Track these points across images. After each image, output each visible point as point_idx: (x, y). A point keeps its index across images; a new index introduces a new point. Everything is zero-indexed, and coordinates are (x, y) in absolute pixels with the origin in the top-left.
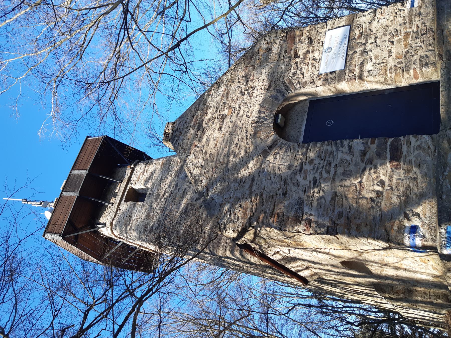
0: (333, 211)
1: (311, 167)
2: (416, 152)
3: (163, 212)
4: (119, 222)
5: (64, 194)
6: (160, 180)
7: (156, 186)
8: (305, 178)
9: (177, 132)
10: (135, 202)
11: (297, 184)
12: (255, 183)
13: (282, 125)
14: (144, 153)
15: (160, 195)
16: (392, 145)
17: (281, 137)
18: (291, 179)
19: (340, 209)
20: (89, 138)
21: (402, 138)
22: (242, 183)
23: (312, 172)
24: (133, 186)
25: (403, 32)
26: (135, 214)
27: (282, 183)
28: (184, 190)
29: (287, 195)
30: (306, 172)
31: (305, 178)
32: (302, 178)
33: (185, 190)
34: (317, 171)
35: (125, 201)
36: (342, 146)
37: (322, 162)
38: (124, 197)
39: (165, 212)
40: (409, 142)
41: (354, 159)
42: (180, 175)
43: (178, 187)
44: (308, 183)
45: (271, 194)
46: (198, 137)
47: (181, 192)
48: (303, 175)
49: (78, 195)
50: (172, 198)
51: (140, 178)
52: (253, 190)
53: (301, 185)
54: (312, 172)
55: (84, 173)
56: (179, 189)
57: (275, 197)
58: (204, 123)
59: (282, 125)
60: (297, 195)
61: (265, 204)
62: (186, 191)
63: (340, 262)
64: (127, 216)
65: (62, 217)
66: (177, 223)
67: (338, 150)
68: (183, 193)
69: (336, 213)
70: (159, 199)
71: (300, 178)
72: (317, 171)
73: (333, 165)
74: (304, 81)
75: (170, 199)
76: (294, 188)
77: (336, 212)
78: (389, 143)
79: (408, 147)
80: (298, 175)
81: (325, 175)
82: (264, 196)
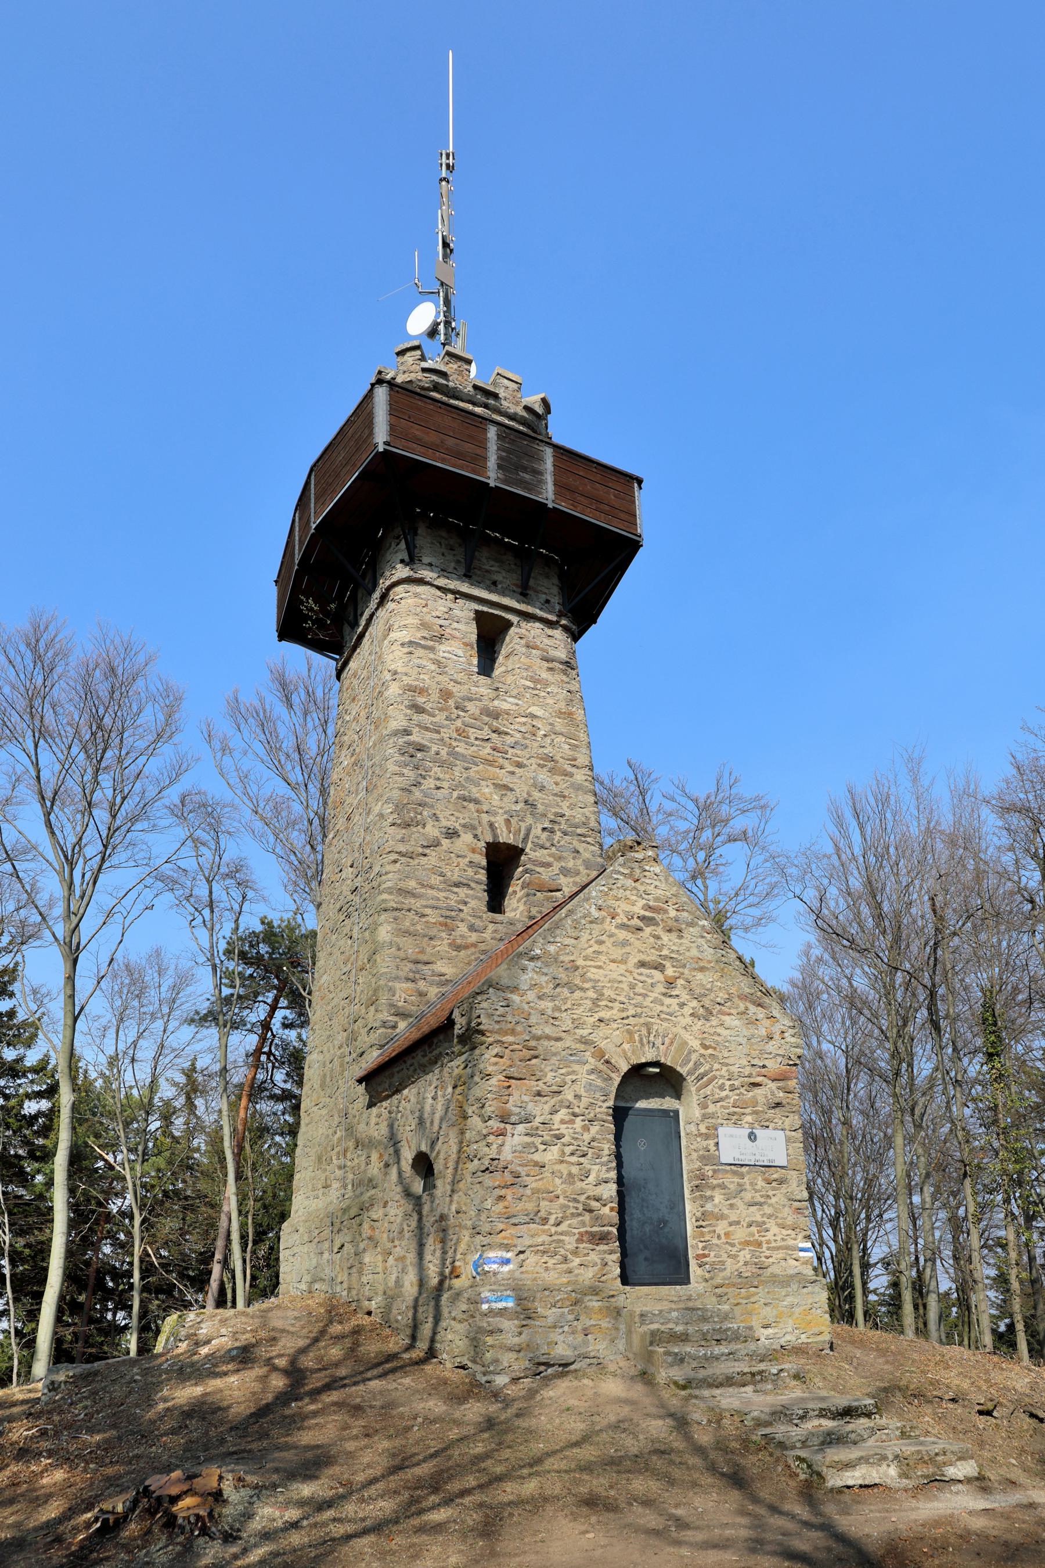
0: (520, 1165)
1: (579, 1130)
2: (599, 1261)
3: (459, 735)
4: (426, 605)
5: (492, 432)
6: (530, 713)
7: (517, 705)
8: (562, 1122)
9: (638, 871)
10: (475, 646)
11: (554, 1112)
12: (553, 1043)
13: (643, 1072)
14: (595, 622)
15: (497, 719)
16: (609, 1233)
17: (623, 1077)
18: (561, 1101)
19: (523, 1174)
20: (636, 485)
21: (617, 1244)
22: (552, 1021)
23: (571, 1131)
24: (513, 631)
25: (763, 1239)
26: (449, 652)
27: (555, 1088)
28: (511, 786)
29: (537, 1098)
30: (572, 1122)
31: (562, 1122)
32: (563, 1117)
33: (512, 790)
34: (573, 1138)
35: (477, 612)
36: (608, 1170)
37: (586, 1143)
38: (485, 609)
39: (459, 741)
40: (611, 1252)
41: (590, 1186)
42: (545, 769)
43: (517, 770)
44: (555, 1127)
45: (537, 1073)
46: (629, 920)
47: (507, 780)
48: (567, 1118)
49: (492, 484)
50: (490, 758)
51: (534, 651)
52: (542, 1042)
53: (553, 1117)
54: (571, 1131)
55: (548, 494)
56: (513, 773)
57: (533, 1078)
58: (653, 928)
59: (643, 1072)
60: (538, 1113)
61: (523, 1064)
62: (509, 793)
63: (371, 1105)
64: (441, 626)
65: (433, 438)
66: (439, 779)
67: (602, 1164)
68: (505, 786)
69: (518, 1168)
70: (486, 719)
71: (563, 1114)
72: (573, 1138)
73: (582, 1160)
74: (709, 1102)
75: (488, 750)
76: (547, 1108)
77: (519, 1169)
78: (610, 1229)
79: (605, 1252)
80: (567, 1110)
81: (568, 1150)
82: (534, 1061)
